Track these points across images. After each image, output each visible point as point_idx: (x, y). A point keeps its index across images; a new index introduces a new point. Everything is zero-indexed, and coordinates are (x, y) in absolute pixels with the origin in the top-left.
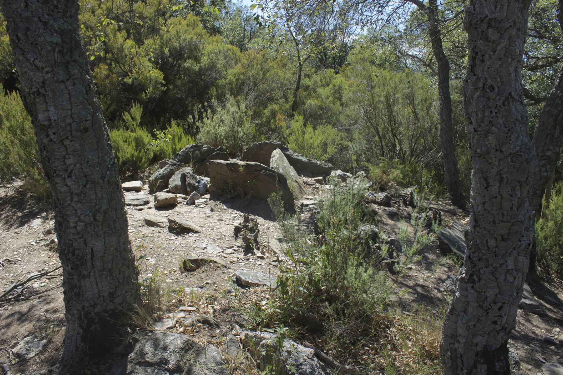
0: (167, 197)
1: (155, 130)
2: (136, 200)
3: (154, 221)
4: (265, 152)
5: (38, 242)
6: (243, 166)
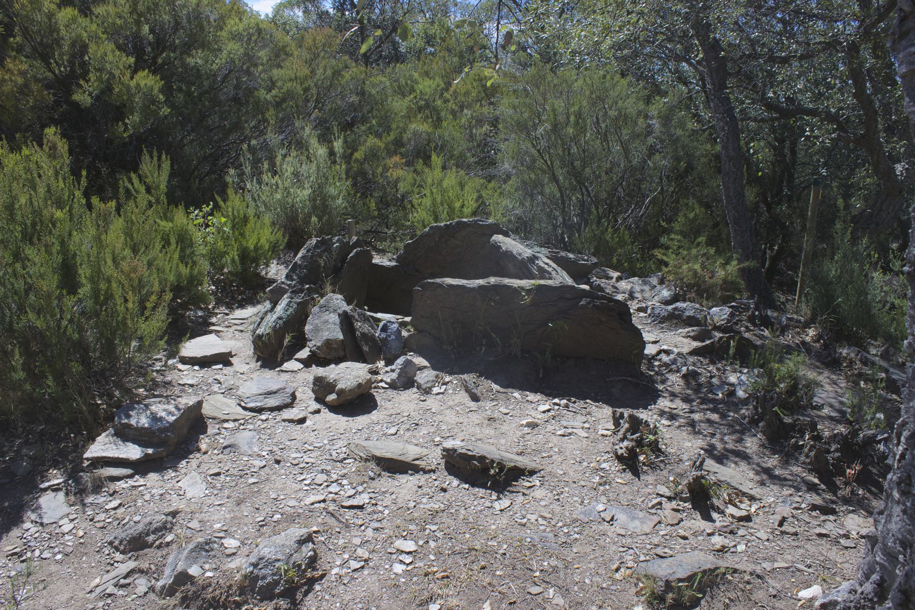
0: (360, 381)
3: (402, 458)
5: (123, 581)
6: (528, 292)
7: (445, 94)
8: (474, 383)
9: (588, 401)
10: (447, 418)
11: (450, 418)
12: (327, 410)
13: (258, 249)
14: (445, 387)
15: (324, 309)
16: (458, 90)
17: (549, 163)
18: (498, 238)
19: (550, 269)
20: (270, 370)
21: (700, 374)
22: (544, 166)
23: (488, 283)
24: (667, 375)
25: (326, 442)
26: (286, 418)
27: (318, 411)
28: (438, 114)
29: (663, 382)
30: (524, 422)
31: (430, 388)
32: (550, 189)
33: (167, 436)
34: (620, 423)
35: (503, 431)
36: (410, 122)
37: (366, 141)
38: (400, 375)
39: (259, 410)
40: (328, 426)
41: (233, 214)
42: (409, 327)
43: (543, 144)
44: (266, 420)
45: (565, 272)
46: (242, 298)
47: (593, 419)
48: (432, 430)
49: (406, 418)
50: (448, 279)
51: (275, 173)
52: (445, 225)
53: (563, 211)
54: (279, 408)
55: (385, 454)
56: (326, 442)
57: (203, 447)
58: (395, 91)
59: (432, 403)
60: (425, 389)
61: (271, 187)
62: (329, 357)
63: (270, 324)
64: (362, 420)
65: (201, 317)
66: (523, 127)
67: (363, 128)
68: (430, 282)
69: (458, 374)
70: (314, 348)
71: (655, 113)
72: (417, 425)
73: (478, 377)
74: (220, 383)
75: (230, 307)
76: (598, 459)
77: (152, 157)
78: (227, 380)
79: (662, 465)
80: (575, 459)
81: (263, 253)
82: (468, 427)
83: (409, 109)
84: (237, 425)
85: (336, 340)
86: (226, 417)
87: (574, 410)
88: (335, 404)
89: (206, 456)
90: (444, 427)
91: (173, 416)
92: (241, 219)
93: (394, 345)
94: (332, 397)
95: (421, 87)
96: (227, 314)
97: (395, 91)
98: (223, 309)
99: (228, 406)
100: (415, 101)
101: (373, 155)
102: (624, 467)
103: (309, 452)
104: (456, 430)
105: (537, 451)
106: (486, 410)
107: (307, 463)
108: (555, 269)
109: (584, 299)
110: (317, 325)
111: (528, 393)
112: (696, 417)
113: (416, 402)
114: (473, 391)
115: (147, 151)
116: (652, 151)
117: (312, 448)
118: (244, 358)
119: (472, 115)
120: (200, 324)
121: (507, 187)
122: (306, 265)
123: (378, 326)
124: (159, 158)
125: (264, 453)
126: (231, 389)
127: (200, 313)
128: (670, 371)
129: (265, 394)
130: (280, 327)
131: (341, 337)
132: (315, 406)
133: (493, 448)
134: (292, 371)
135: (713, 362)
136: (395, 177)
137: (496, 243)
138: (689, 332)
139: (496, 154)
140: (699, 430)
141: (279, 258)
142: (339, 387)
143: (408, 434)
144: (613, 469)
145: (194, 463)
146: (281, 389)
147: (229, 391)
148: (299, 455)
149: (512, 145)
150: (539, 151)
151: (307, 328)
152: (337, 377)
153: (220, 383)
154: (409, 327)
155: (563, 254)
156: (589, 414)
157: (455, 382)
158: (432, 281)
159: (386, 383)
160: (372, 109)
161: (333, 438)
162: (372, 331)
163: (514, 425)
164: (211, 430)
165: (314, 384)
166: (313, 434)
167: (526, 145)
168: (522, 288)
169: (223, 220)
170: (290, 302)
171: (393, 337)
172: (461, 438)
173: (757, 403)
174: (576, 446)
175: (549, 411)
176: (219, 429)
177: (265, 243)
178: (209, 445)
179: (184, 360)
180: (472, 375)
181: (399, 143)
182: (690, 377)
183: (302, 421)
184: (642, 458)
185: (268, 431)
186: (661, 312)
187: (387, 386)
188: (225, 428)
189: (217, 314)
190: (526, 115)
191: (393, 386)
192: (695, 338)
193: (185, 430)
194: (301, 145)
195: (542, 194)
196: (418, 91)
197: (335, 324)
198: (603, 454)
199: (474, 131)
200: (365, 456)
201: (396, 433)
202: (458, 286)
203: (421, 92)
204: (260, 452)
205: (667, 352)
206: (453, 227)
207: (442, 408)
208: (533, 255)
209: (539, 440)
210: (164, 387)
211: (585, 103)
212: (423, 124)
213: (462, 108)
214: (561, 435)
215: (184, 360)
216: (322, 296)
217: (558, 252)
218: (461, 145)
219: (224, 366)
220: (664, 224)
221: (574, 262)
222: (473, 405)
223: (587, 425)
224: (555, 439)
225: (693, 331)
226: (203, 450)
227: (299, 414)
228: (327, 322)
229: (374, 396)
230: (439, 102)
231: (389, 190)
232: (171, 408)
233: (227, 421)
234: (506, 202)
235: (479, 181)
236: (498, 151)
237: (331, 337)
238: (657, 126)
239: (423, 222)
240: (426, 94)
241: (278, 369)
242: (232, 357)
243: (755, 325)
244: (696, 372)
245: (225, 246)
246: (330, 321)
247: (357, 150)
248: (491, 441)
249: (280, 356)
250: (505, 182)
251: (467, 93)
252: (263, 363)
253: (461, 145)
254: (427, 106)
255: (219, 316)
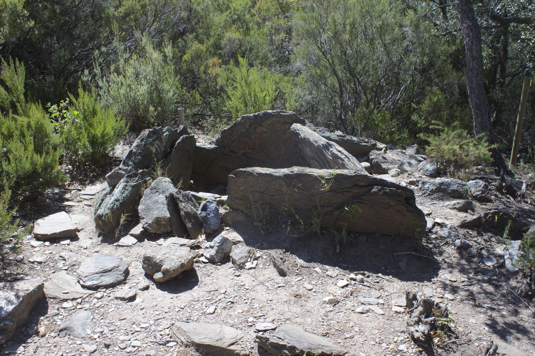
1: (49, 104)
2: (105, 272)
4: (265, 129)
6: (328, 181)
7: (252, 10)
8: (281, 259)
9: (380, 275)
10: (259, 294)
11: (261, 294)
12: (155, 286)
13: (104, 136)
14: (256, 262)
15: (154, 191)
16: (262, 8)
17: (331, 61)
18: (296, 126)
19: (343, 157)
20: (109, 244)
21: (471, 246)
22: (326, 64)
23: (292, 172)
24: (444, 248)
25: (152, 322)
26: (118, 296)
27: (147, 288)
28: (247, 25)
29: (441, 253)
30: (327, 299)
31: (244, 263)
32: (332, 81)
33: (5, 324)
34: (413, 304)
35: (309, 308)
36: (226, 31)
37: (191, 46)
38: (217, 252)
39: (96, 288)
40: (154, 304)
41: (84, 108)
42: (225, 206)
43: (326, 47)
44: (101, 298)
45: (355, 158)
46: (93, 175)
47: (386, 294)
48: (246, 309)
49: (223, 295)
50: (258, 168)
51: (119, 74)
52: (254, 116)
53: (341, 96)
54: (113, 286)
55: (203, 340)
56: (152, 322)
57: (42, 329)
58: (216, 9)
59: (246, 278)
60: (240, 265)
61: (118, 84)
62: (158, 232)
63: (109, 206)
64: (185, 296)
65: (57, 194)
66: (312, 35)
67: (191, 36)
68: (242, 171)
69: (267, 249)
70: (147, 225)
71: (408, 22)
72: (232, 303)
73: (284, 252)
74: (65, 260)
75: (83, 183)
76: (395, 340)
77: (9, 65)
78: (70, 257)
79: (454, 346)
80: (374, 340)
81: (109, 138)
82: (277, 304)
83: (226, 21)
84: (75, 304)
85: (164, 218)
86: (65, 296)
87: (368, 284)
88: (162, 281)
89: (44, 339)
90: (256, 305)
91: (12, 304)
92: (90, 112)
93: (213, 222)
94: (158, 276)
95: (234, 5)
96: (80, 190)
97: (216, 9)
98: (77, 186)
99: (69, 284)
100: (230, 16)
101: (198, 57)
102: (421, 349)
103: (136, 333)
104: (266, 308)
105: (341, 331)
106: (293, 286)
107: (134, 347)
108: (347, 156)
109: (376, 187)
110: (148, 205)
111: (327, 267)
112: (475, 289)
113: (232, 277)
114: (280, 267)
115: (4, 60)
116: (407, 51)
117: (139, 329)
118: (88, 232)
119: (272, 26)
120: (57, 200)
121: (298, 80)
122: (140, 153)
123: (200, 204)
124: (15, 63)
125: (96, 336)
126: (74, 265)
127: (57, 191)
128: (447, 243)
129: (101, 272)
130: (117, 209)
131: (169, 216)
132: (145, 282)
133: (299, 330)
134: (127, 246)
135: (480, 234)
136: (214, 74)
137: (295, 130)
138: (455, 205)
139: (290, 54)
140: (479, 304)
141: (126, 140)
142: (164, 267)
143: (225, 312)
144: (410, 351)
145: (31, 347)
146: (115, 267)
147: (72, 268)
148: (127, 338)
149: (303, 49)
150: (323, 53)
151: (140, 207)
152: (162, 258)
153: (65, 260)
154: (225, 206)
155: (348, 137)
156: (382, 288)
157: (265, 257)
158: (244, 169)
159: (206, 258)
160: (199, 21)
161: (159, 317)
162: (195, 210)
163: (318, 302)
164: (51, 311)
165: (144, 262)
166: (141, 312)
167: (314, 49)
168: (322, 177)
169: (76, 113)
170: (126, 185)
171: (212, 215)
172: (270, 319)
173: (530, 280)
174: (374, 324)
175: (347, 286)
176: (58, 309)
177: (110, 131)
178: (47, 327)
179: (38, 238)
180: (280, 251)
181: (217, 46)
182: (463, 249)
183: (132, 299)
184: (436, 340)
185: (102, 310)
186: (430, 186)
187: (207, 261)
188: (64, 308)
189: (70, 191)
190: (313, 26)
191: (212, 261)
192: (460, 210)
193: (26, 315)
194: (141, 53)
195: (326, 85)
196: (232, 9)
197: (163, 204)
198: (399, 334)
199: (274, 37)
200: (185, 343)
201: (214, 312)
202: (266, 174)
203: (234, 9)
204: (92, 335)
205: (441, 225)
206: (260, 117)
207: (254, 284)
208: (328, 143)
209: (341, 318)
210: (16, 265)
211: (357, 16)
212: (235, 33)
213: (264, 20)
214: (359, 313)
215: (38, 238)
216: (154, 179)
217: (345, 136)
218: (265, 49)
219: (71, 241)
220: (414, 105)
221: (358, 144)
222: (280, 279)
223: (381, 301)
224: (354, 317)
225: (458, 203)
226: (41, 334)
227: (130, 292)
228: (156, 202)
229: (195, 271)
230: (248, 16)
231: (210, 83)
232: (11, 295)
233: (66, 300)
234: (297, 91)
235: (278, 76)
236: (291, 52)
237: (160, 215)
238: (410, 32)
239: (236, 107)
240: (238, 10)
241: (115, 244)
242: (79, 231)
243: (502, 194)
244: (468, 244)
245: (78, 134)
246: (160, 201)
247: (185, 54)
248: (298, 320)
249: (117, 232)
250: (297, 75)
251: (268, 10)
252: (103, 238)
253: (265, 49)
254: (239, 19)
255: (73, 192)
